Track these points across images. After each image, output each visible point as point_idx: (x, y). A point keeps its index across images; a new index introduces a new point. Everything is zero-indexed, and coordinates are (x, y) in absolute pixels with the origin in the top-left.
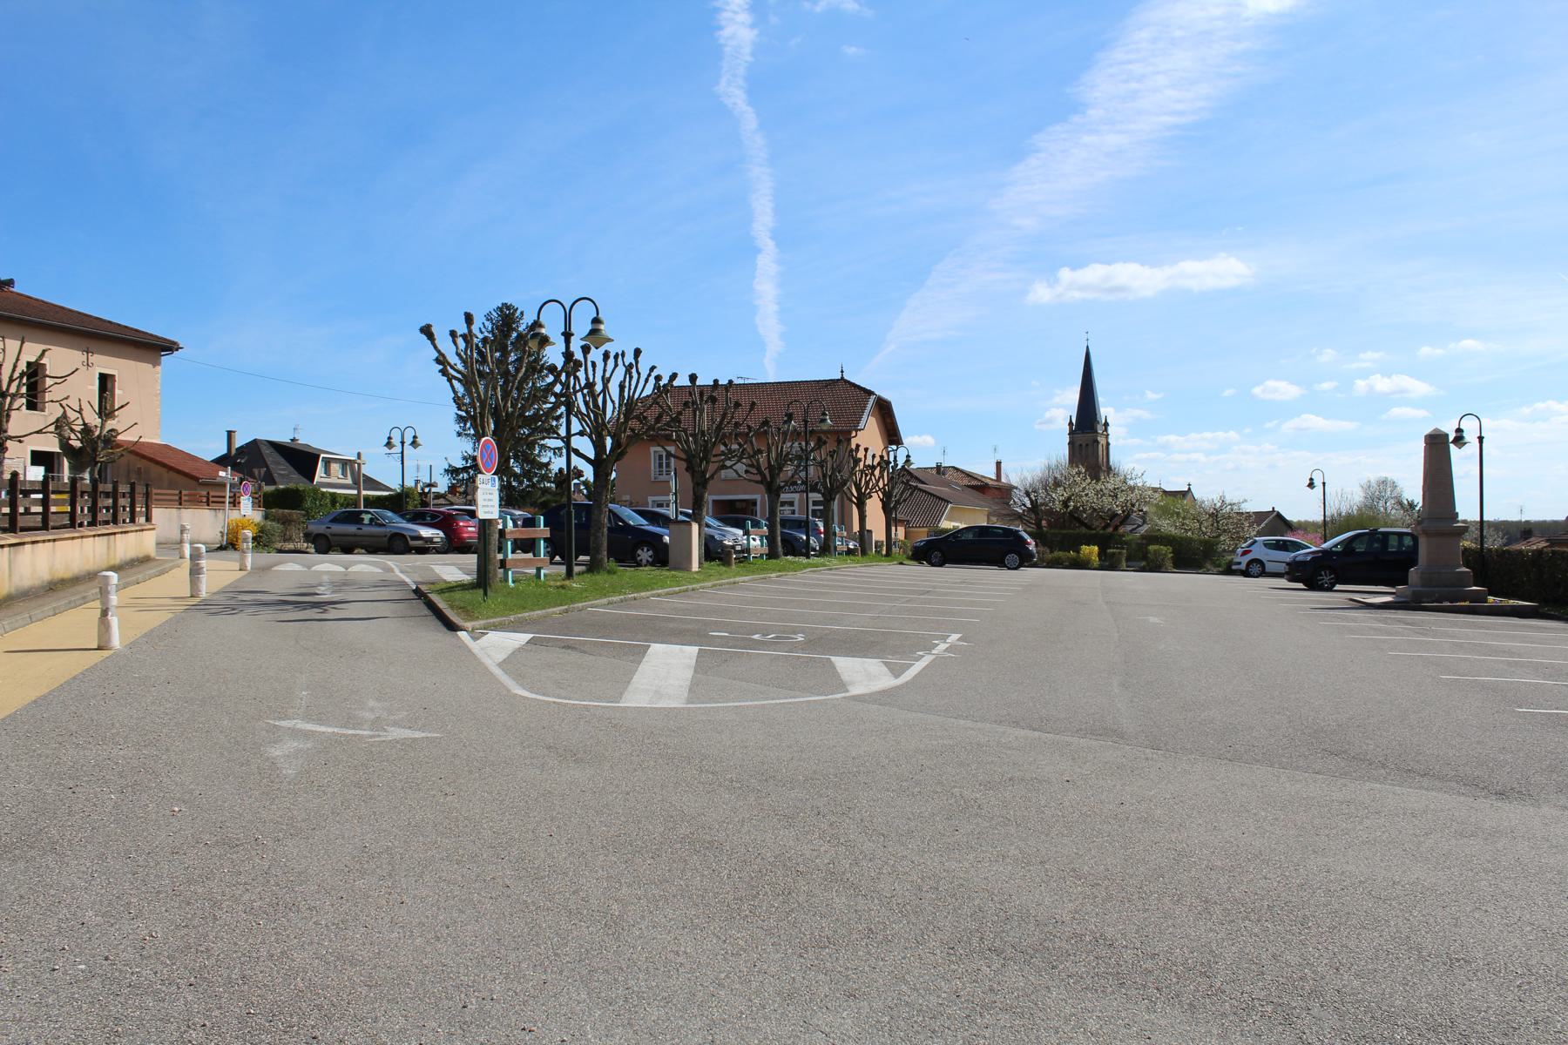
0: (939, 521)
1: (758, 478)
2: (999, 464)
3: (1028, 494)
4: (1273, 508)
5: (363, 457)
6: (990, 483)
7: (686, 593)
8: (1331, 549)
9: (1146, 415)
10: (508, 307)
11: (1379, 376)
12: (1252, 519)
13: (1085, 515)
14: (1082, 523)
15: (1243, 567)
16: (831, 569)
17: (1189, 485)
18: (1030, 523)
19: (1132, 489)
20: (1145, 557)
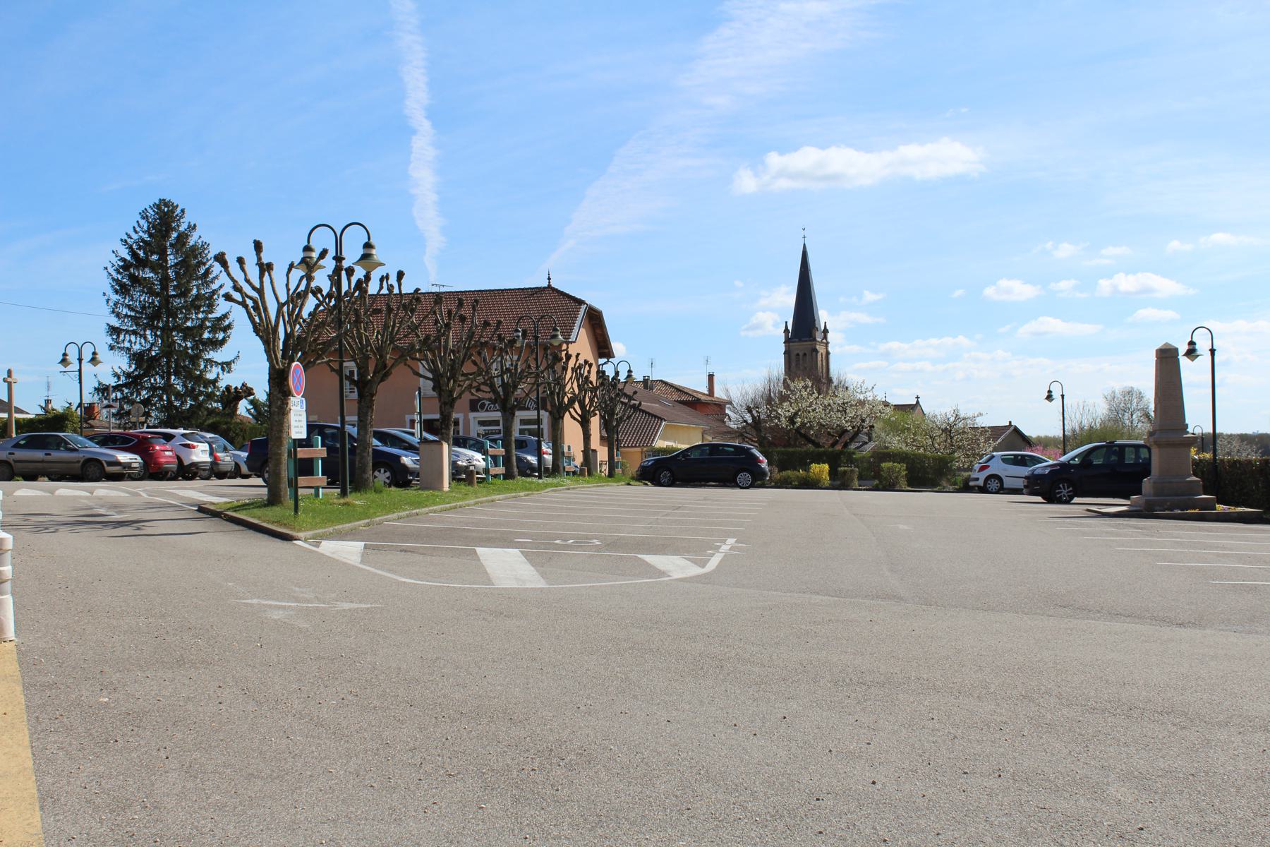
0: (653, 440)
1: (491, 395)
2: (711, 377)
3: (749, 410)
4: (1010, 422)
5: (14, 376)
6: (703, 398)
7: (418, 517)
8: (1069, 461)
9: (864, 318)
10: (164, 202)
11: (1122, 274)
12: (988, 434)
13: (812, 432)
14: (809, 440)
15: (981, 483)
16: (569, 489)
17: (918, 398)
18: (752, 441)
19: (862, 403)
20: (877, 475)
